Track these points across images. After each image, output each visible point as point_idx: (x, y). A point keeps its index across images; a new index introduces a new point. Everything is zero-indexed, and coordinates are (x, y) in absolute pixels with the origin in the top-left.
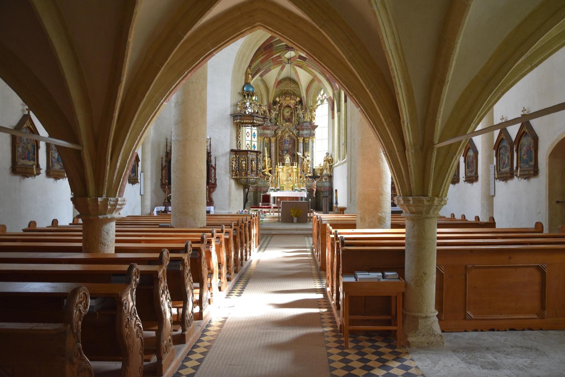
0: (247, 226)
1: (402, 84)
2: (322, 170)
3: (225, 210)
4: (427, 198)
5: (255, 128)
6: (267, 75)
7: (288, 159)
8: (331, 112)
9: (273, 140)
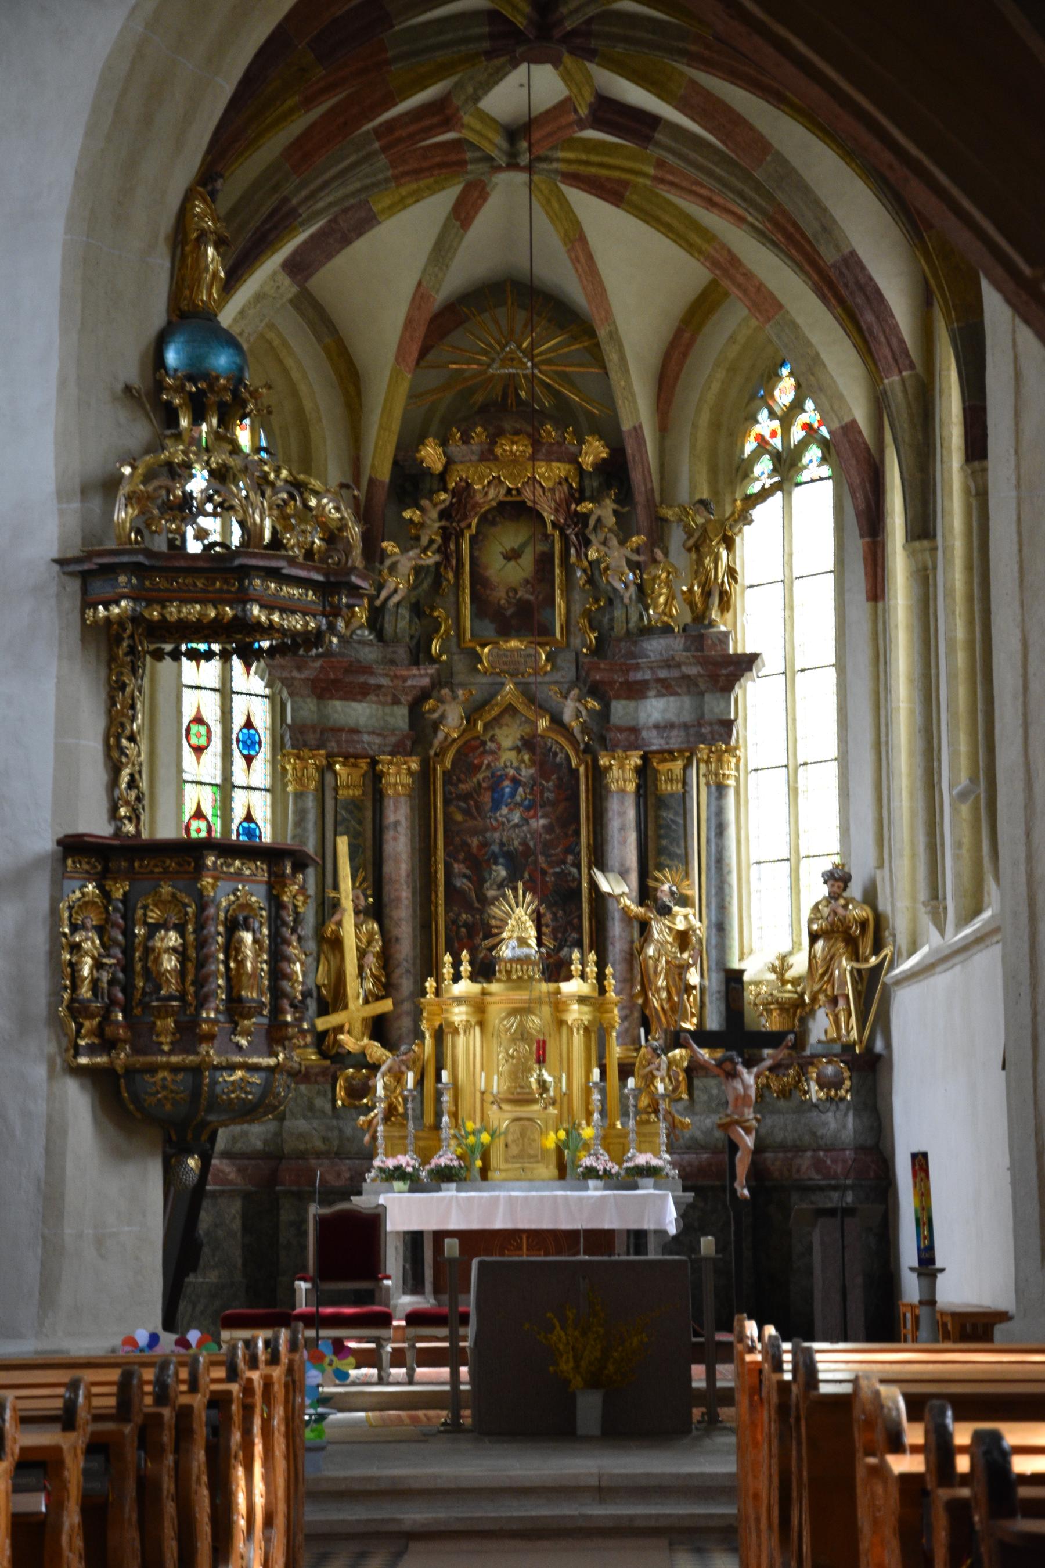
2: (798, 1010)
6: (340, 261)
7: (518, 930)
8: (857, 545)
9: (399, 775)
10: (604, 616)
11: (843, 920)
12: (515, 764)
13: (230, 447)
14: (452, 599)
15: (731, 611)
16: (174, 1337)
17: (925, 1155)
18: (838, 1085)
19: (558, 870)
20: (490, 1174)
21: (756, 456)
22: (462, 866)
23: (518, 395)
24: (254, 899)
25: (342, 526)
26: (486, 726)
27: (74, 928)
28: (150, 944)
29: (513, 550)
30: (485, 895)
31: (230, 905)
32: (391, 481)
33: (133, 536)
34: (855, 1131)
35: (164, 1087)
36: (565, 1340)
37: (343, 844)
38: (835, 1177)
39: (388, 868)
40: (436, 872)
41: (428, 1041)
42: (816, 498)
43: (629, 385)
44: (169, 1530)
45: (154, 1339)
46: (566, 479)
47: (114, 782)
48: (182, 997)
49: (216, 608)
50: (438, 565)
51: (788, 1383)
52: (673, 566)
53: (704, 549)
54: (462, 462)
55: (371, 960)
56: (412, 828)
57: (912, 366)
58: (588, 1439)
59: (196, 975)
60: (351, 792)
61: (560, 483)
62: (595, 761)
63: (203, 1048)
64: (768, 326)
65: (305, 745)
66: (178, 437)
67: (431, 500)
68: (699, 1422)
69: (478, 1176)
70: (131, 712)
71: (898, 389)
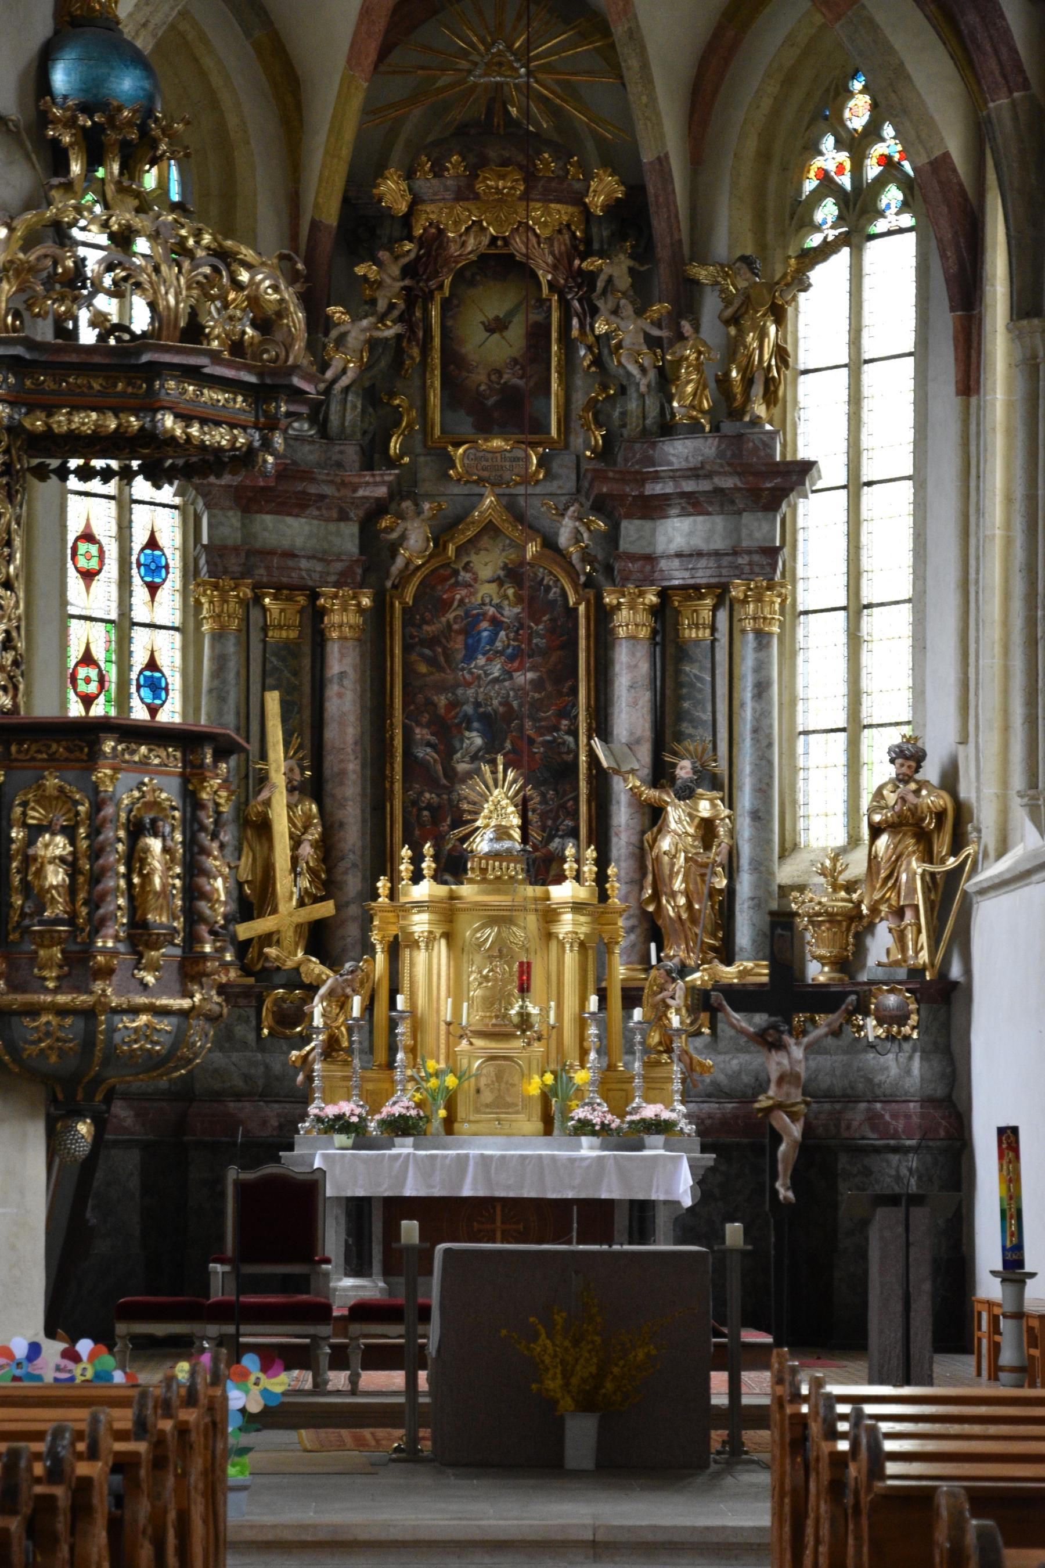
0: (102, 1504)
5: (167, 493)
7: (497, 812)
8: (945, 321)
9: (344, 616)
10: (614, 407)
11: (914, 810)
12: (496, 601)
13: (136, 203)
14: (417, 382)
15: (780, 405)
16: (61, 1346)
17: (1015, 1130)
18: (901, 1019)
19: (548, 738)
20: (456, 1126)
21: (817, 197)
22: (425, 731)
23: (507, 113)
24: (164, 795)
25: (281, 312)
26: (459, 550)
28: (31, 851)
29: (497, 319)
30: (454, 769)
31: (133, 804)
32: (339, 226)
33: (9, 319)
34: (922, 1079)
35: (48, 1034)
36: (551, 1345)
37: (273, 700)
38: (895, 1136)
39: (331, 734)
40: (392, 739)
41: (380, 958)
42: (894, 260)
43: (653, 99)
45: (35, 1350)
46: (568, 226)
48: (71, 919)
49: (117, 416)
50: (399, 337)
51: (843, 1453)
52: (705, 344)
53: (746, 323)
54: (433, 201)
55: (306, 850)
56: (362, 680)
57: (1026, 85)
58: (578, 1474)
59: (90, 892)
60: (284, 634)
61: (560, 231)
62: (599, 598)
63: (98, 986)
64: (837, 26)
65: (226, 572)
66: (68, 187)
67: (391, 250)
68: (719, 1453)
69: (442, 1130)
70: (6, 551)
71: (1006, 116)
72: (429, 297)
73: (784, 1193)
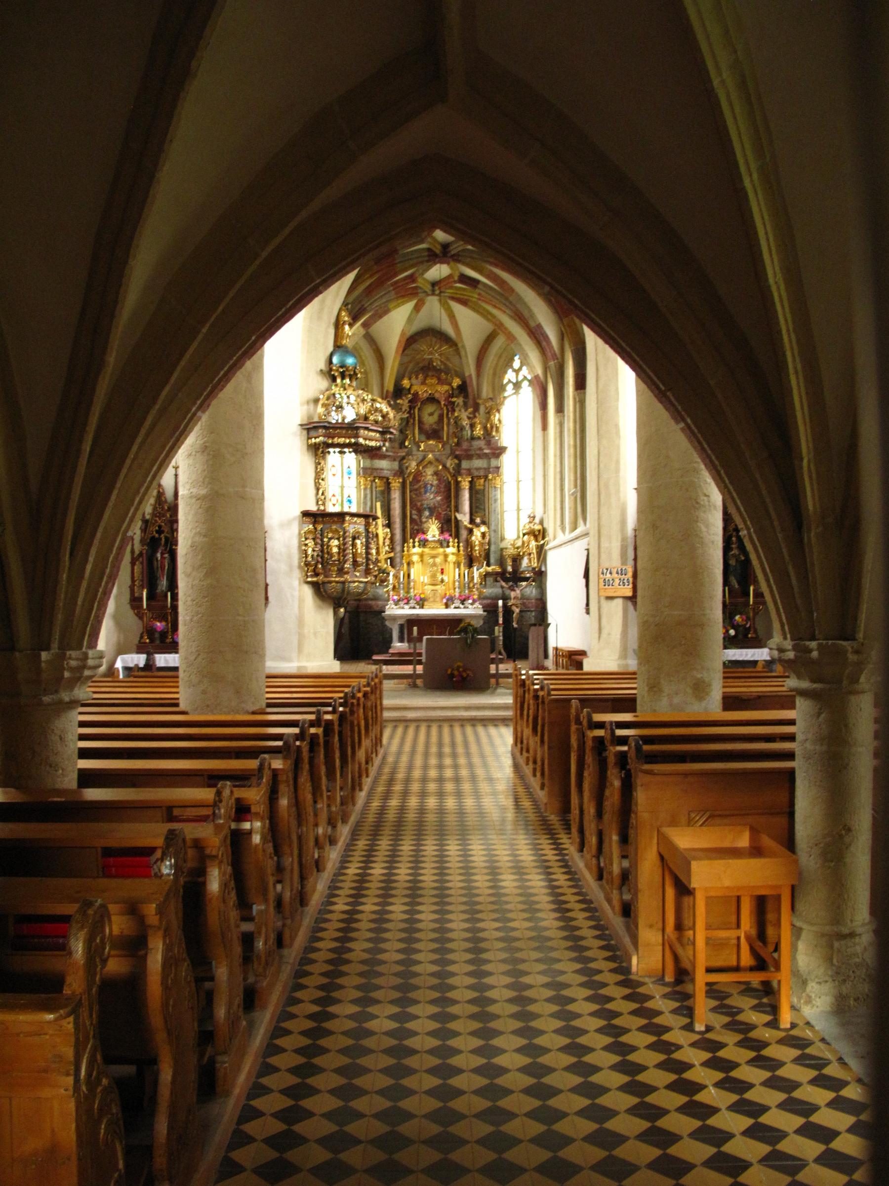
1: (799, 367)
3: (289, 660)
4: (855, 644)
8: (539, 414)
9: (396, 484)
21: (507, 383)
25: (387, 413)
26: (423, 468)
27: (306, 539)
37: (378, 504)
43: (468, 362)
44: (356, 735)
47: (317, 494)
72: (414, 408)
73: (515, 625)
